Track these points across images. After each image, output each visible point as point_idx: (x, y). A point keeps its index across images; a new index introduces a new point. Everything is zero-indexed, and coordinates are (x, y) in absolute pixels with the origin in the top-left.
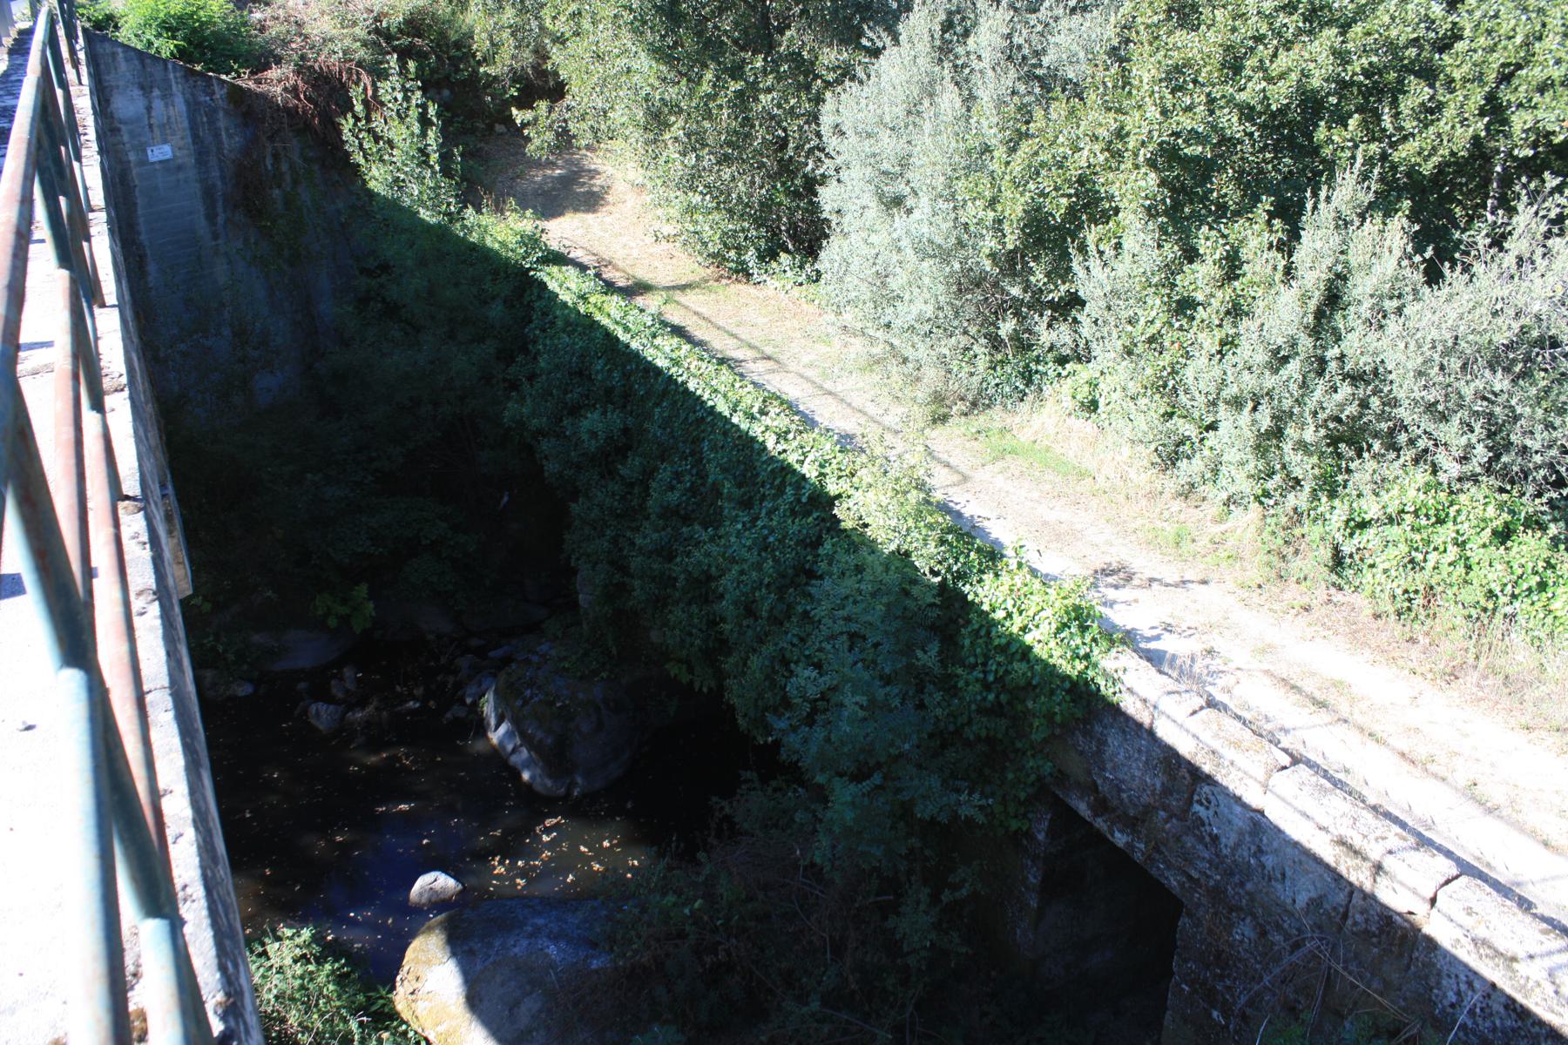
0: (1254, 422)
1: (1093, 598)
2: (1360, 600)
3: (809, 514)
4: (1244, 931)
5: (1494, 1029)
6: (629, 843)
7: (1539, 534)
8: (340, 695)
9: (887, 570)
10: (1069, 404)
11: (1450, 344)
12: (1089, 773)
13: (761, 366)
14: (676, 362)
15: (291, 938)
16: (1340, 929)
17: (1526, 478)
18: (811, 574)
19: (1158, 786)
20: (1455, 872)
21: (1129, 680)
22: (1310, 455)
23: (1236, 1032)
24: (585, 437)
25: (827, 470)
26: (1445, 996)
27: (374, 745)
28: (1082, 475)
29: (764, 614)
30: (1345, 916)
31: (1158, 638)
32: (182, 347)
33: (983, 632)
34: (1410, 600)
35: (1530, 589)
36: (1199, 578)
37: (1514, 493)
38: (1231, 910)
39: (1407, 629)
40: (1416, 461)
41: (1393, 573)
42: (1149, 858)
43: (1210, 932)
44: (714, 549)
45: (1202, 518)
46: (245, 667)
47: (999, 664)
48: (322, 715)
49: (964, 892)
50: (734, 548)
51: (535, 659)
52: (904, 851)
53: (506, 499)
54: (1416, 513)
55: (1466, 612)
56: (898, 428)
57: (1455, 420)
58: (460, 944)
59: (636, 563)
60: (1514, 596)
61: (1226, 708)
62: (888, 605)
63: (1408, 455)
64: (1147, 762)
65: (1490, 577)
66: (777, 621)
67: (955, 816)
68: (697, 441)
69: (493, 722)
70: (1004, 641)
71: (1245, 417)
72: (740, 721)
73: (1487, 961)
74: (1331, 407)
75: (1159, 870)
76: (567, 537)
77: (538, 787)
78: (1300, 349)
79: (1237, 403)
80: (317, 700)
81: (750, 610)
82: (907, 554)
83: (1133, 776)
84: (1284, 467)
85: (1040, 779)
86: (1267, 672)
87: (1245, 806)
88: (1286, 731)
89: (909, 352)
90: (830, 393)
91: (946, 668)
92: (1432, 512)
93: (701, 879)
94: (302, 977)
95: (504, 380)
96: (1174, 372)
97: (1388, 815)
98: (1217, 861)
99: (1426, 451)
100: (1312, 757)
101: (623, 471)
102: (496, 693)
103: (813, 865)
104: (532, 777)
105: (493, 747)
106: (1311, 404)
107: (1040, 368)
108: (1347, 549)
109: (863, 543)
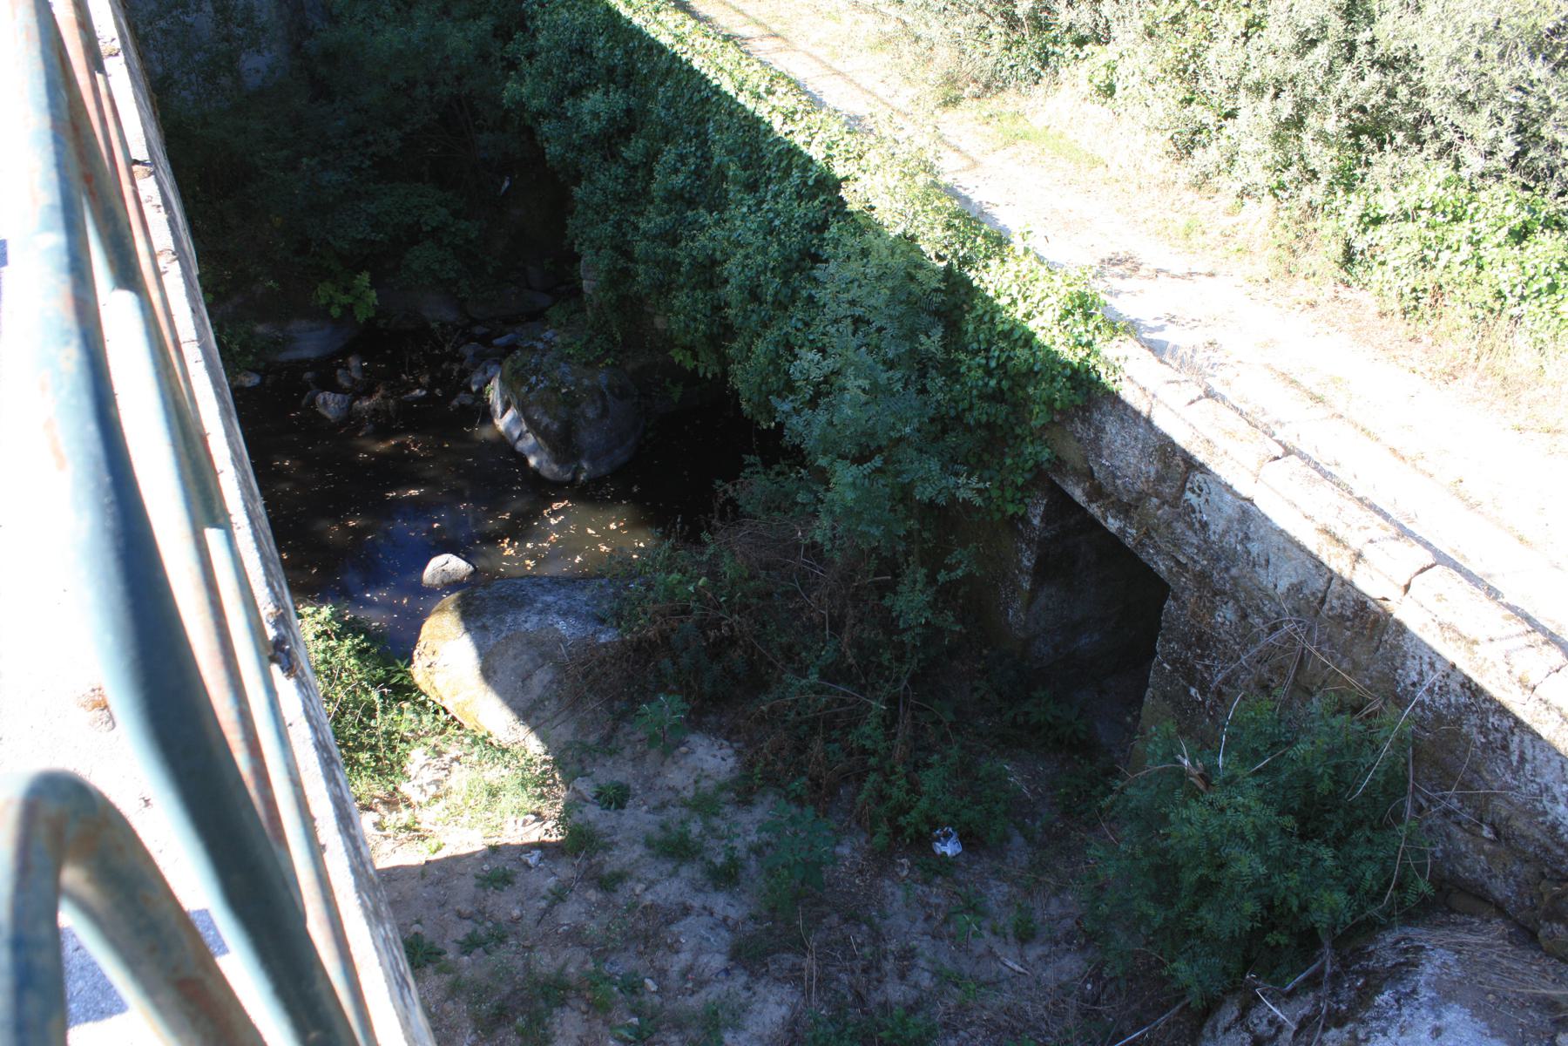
0: (1274, 110)
1: (1098, 286)
2: (1368, 299)
3: (815, 197)
4: (1226, 614)
5: (1449, 706)
6: (635, 524)
7: (1557, 234)
8: (347, 384)
9: (893, 254)
10: (1086, 88)
11: (1490, 28)
12: (1086, 460)
13: (770, 43)
14: (680, 39)
15: (312, 615)
16: (1317, 612)
17: (1552, 176)
18: (816, 258)
19: (1153, 473)
20: (1431, 561)
21: (1129, 368)
22: (1330, 146)
23: (1211, 707)
24: (587, 118)
25: (834, 152)
26: (1408, 676)
27: (382, 433)
28: (1094, 163)
29: (769, 298)
30: (1323, 602)
31: (1161, 329)
32: (162, 23)
33: (987, 318)
34: (1417, 299)
35: (1539, 291)
36: (1208, 270)
37: (1537, 191)
38: (1216, 594)
39: (1412, 327)
40: (1440, 154)
41: (1403, 271)
42: (1140, 543)
43: (1194, 615)
44: (719, 233)
45: (1214, 210)
46: (251, 358)
47: (1002, 350)
48: (330, 404)
49: (960, 573)
50: (739, 233)
51: (540, 345)
52: (902, 533)
53: (506, 184)
54: (1433, 210)
55: (1472, 313)
56: (908, 110)
57: (1485, 112)
58: (471, 615)
59: (640, 247)
60: (1523, 297)
61: (1223, 399)
62: (893, 289)
63: (1432, 148)
64: (1142, 450)
65: (1502, 277)
66: (780, 305)
67: (953, 499)
68: (702, 121)
69: (499, 409)
70: (1007, 327)
71: (1266, 103)
72: (744, 405)
73: (1451, 644)
74: (1356, 96)
75: (1148, 555)
76: (569, 221)
77: (545, 473)
78: (1330, 32)
79: (1258, 89)
80: (324, 389)
81: (754, 294)
82: (913, 238)
83: (1126, 461)
84: (1302, 158)
85: (1037, 465)
86: (1267, 366)
87: (1235, 494)
88: (1282, 425)
89: (921, 30)
90: (839, 73)
91: (948, 353)
92: (1449, 209)
93: (705, 558)
94: (324, 651)
95: (503, 58)
96: (1196, 55)
97: (1372, 507)
98: (1205, 547)
99: (1450, 145)
100: (1306, 450)
101: (627, 154)
102: (502, 379)
103: (814, 545)
104: (539, 463)
105: (500, 433)
106: (1336, 91)
107: (1057, 49)
108: (1359, 245)
109: (869, 226)
